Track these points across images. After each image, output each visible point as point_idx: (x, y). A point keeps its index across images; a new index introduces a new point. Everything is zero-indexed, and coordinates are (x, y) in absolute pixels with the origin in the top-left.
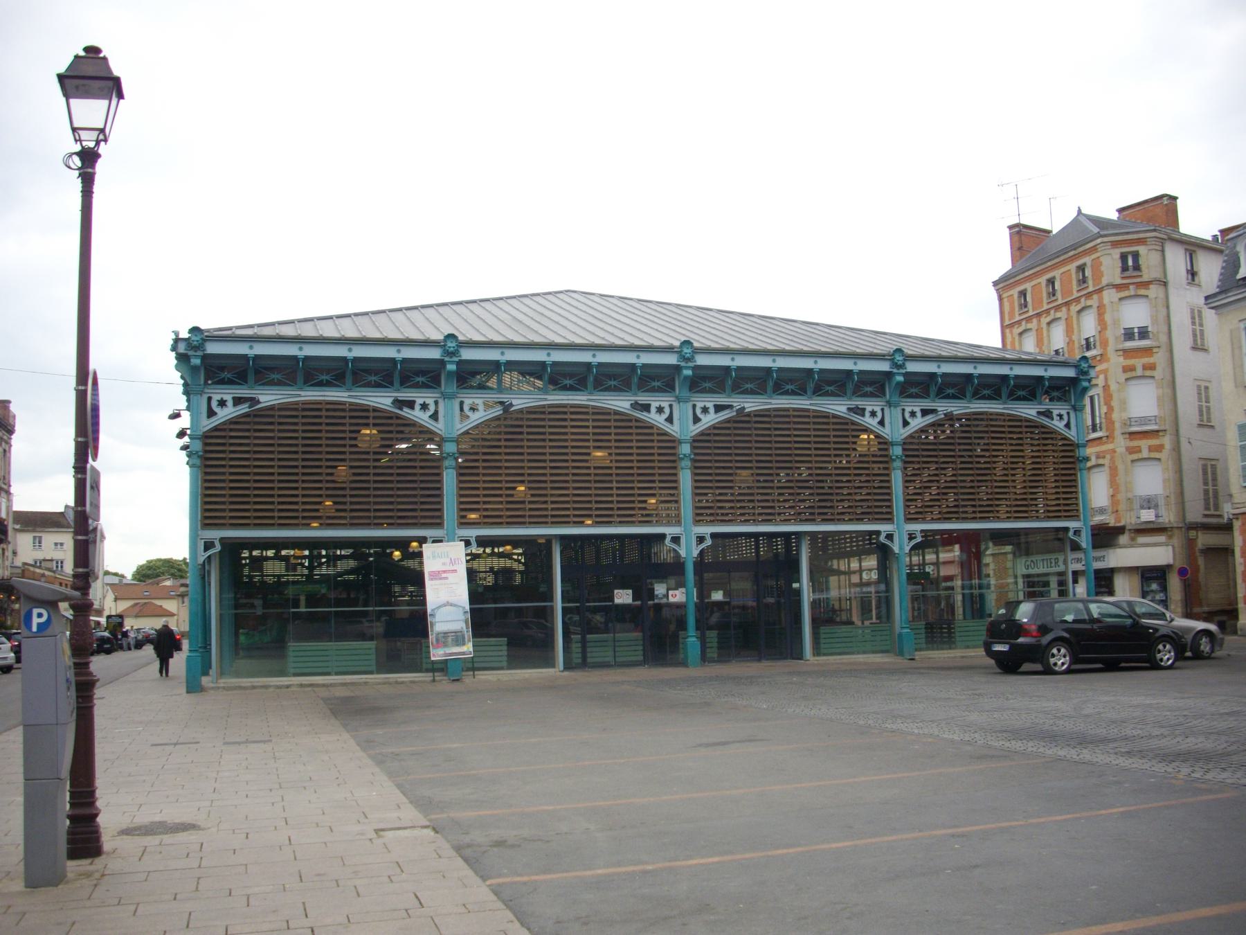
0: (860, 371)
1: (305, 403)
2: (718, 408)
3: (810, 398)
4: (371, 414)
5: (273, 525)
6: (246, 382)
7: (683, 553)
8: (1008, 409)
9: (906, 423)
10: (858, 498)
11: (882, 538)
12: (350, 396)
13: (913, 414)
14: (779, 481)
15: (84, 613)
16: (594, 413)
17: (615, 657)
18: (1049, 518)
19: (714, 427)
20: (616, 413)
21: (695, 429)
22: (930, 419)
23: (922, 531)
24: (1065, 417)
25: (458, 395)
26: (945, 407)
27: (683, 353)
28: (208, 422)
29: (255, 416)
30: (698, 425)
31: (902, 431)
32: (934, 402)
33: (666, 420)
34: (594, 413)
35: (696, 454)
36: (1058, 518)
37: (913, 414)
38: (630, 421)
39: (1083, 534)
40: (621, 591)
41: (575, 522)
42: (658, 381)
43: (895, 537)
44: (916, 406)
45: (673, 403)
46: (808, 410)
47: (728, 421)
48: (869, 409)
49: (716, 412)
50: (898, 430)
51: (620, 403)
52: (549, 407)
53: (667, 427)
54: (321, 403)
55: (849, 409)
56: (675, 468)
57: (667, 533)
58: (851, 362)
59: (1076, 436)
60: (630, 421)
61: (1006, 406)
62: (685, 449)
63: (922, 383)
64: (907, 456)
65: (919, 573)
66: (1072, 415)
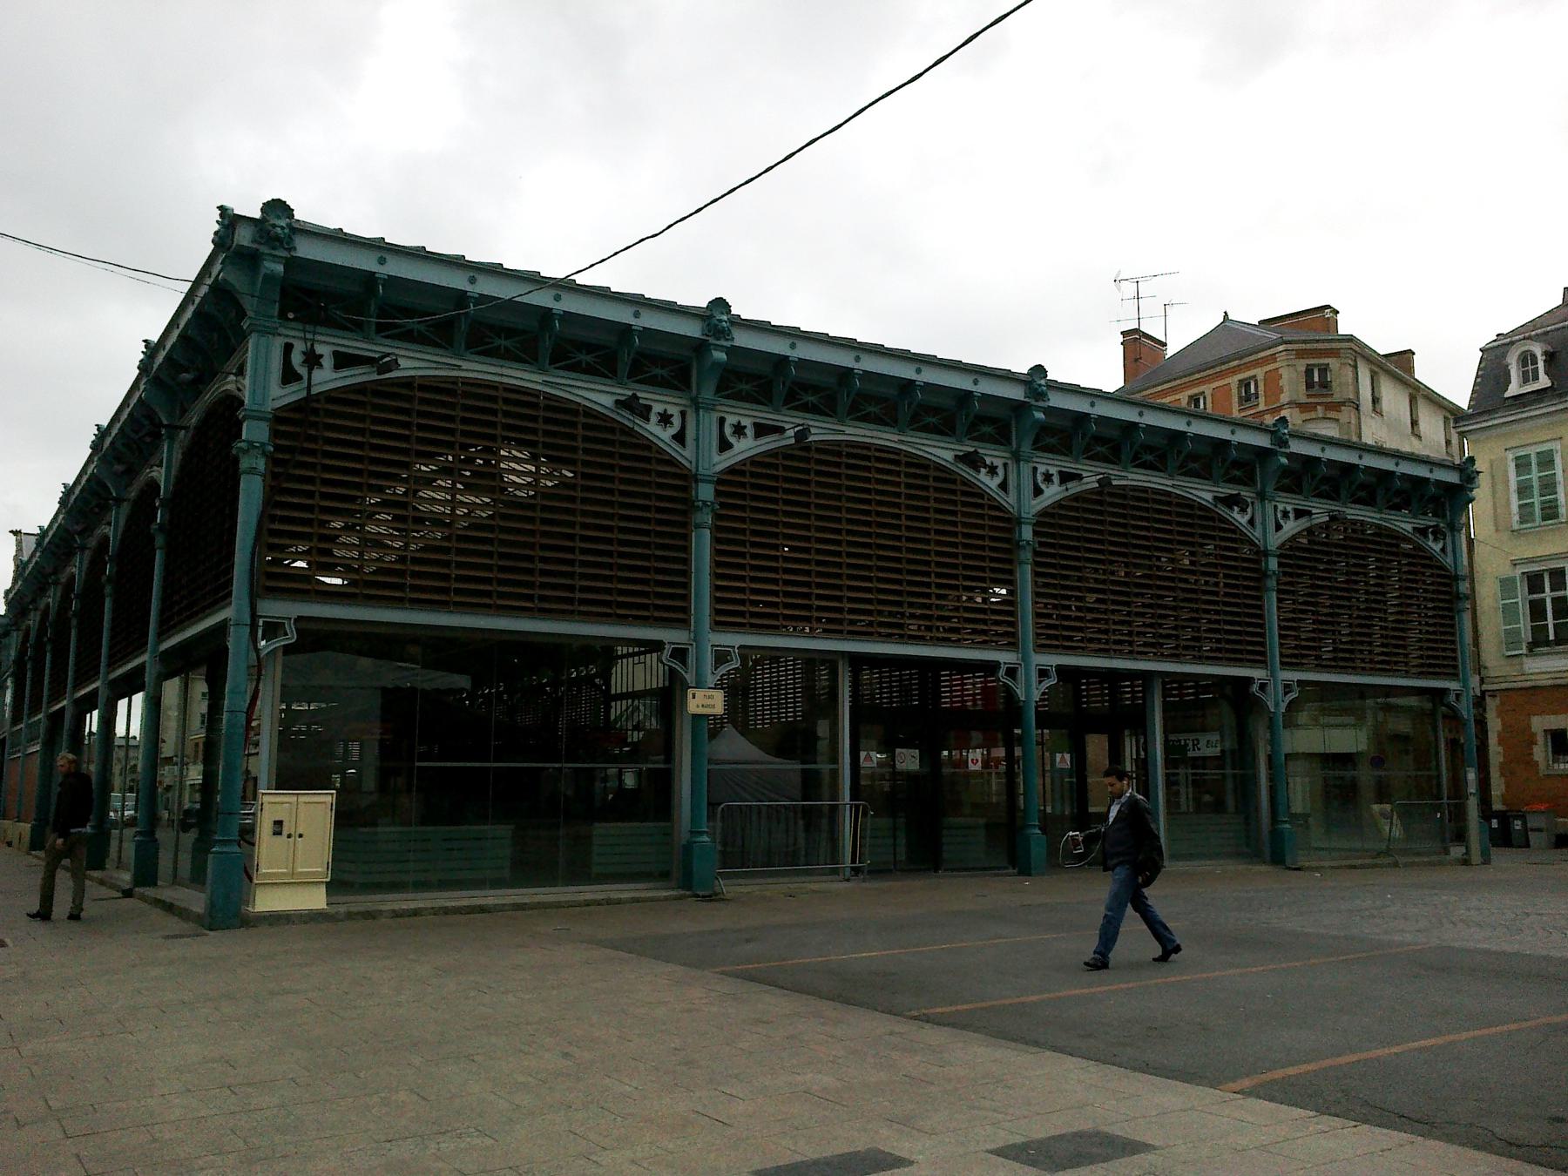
0: (1403, 474)
1: (467, 382)
2: (1066, 477)
3: (542, 371)
4: (932, 473)
5: (401, 600)
6: (771, 401)
7: (1020, 693)
8: (902, 442)
9: (725, 446)
10: (1116, 618)
11: (1255, 688)
12: (546, 383)
13: (1285, 514)
14: (1350, 616)
15: (201, 757)
16: (908, 465)
17: (895, 854)
18: (1420, 675)
19: (753, 461)
20: (589, 413)
21: (722, 462)
22: (1304, 523)
23: (299, 619)
24: (677, 421)
25: (719, 408)
26: (1091, 476)
27: (714, 321)
28: (283, 392)
29: (376, 393)
30: (727, 454)
31: (716, 458)
32: (1077, 462)
33: (674, 437)
34: (908, 465)
35: (722, 505)
36: (1436, 675)
37: (739, 430)
38: (954, 482)
39: (1464, 699)
40: (904, 750)
41: (456, 604)
42: (662, 368)
43: (1268, 688)
44: (1051, 465)
45: (1009, 462)
46: (1169, 494)
47: (360, 389)
48: (657, 408)
49: (1297, 518)
50: (710, 457)
51: (600, 396)
52: (847, 446)
53: (674, 450)
54: (496, 388)
55: (1414, 529)
56: (684, 525)
57: (1002, 661)
58: (971, 378)
59: (1261, 537)
60: (612, 430)
61: (903, 438)
62: (706, 492)
63: (760, 377)
64: (722, 505)
65: (795, 721)
66: (1012, 467)
